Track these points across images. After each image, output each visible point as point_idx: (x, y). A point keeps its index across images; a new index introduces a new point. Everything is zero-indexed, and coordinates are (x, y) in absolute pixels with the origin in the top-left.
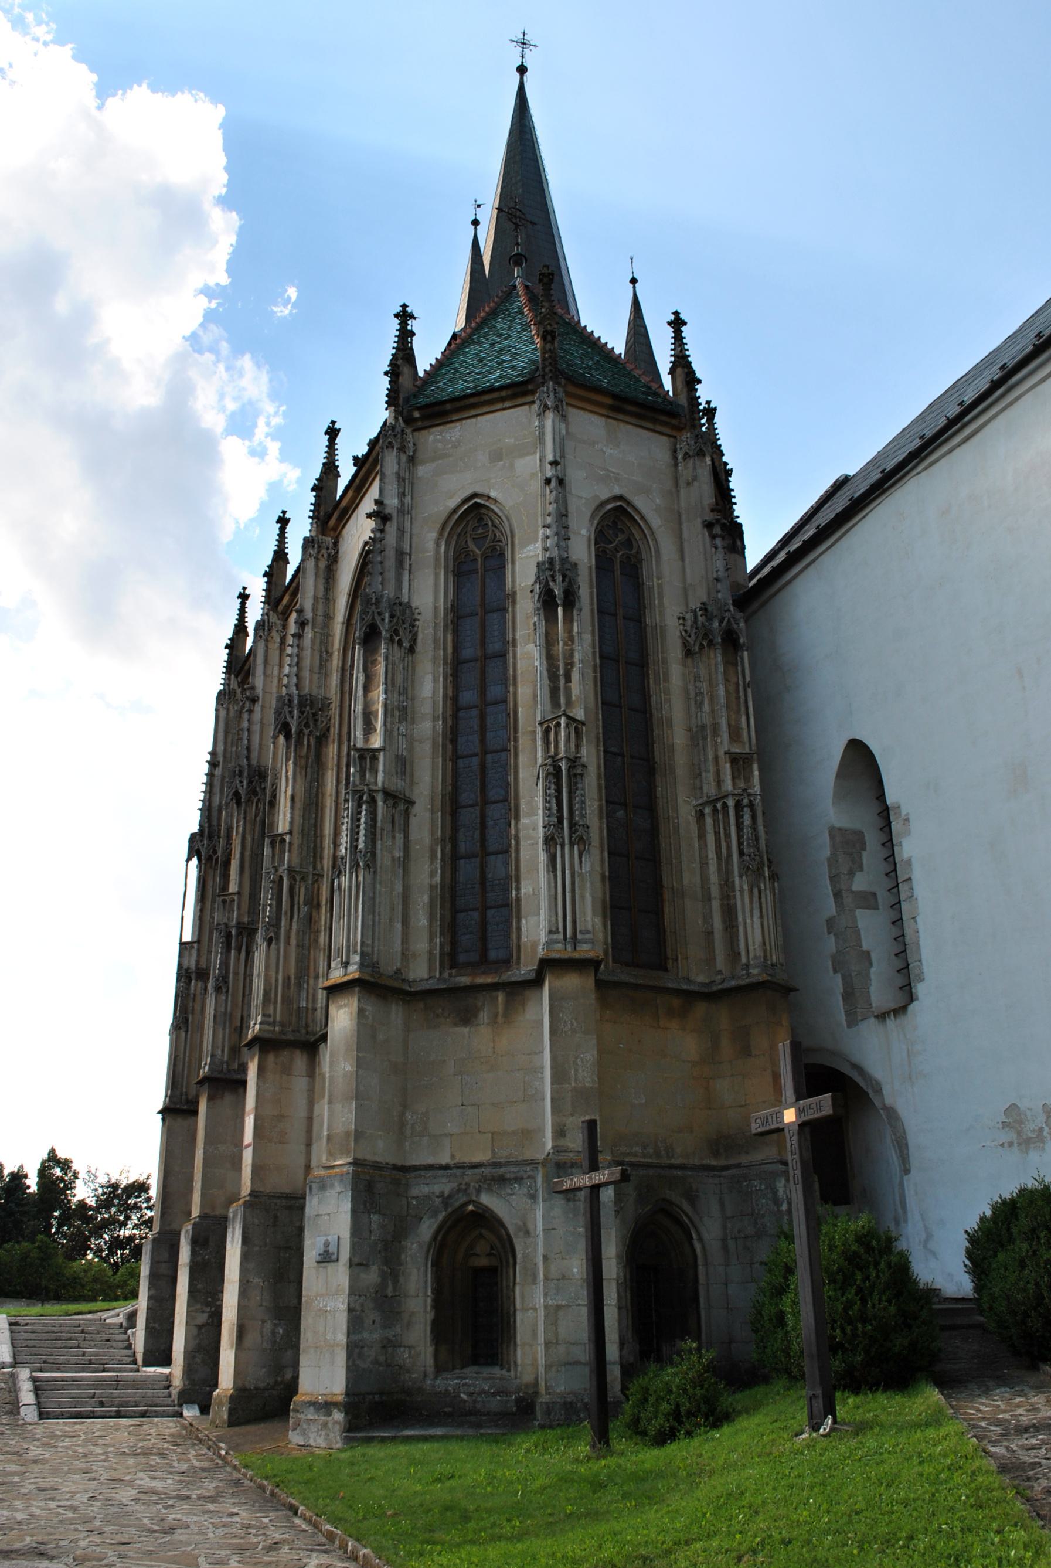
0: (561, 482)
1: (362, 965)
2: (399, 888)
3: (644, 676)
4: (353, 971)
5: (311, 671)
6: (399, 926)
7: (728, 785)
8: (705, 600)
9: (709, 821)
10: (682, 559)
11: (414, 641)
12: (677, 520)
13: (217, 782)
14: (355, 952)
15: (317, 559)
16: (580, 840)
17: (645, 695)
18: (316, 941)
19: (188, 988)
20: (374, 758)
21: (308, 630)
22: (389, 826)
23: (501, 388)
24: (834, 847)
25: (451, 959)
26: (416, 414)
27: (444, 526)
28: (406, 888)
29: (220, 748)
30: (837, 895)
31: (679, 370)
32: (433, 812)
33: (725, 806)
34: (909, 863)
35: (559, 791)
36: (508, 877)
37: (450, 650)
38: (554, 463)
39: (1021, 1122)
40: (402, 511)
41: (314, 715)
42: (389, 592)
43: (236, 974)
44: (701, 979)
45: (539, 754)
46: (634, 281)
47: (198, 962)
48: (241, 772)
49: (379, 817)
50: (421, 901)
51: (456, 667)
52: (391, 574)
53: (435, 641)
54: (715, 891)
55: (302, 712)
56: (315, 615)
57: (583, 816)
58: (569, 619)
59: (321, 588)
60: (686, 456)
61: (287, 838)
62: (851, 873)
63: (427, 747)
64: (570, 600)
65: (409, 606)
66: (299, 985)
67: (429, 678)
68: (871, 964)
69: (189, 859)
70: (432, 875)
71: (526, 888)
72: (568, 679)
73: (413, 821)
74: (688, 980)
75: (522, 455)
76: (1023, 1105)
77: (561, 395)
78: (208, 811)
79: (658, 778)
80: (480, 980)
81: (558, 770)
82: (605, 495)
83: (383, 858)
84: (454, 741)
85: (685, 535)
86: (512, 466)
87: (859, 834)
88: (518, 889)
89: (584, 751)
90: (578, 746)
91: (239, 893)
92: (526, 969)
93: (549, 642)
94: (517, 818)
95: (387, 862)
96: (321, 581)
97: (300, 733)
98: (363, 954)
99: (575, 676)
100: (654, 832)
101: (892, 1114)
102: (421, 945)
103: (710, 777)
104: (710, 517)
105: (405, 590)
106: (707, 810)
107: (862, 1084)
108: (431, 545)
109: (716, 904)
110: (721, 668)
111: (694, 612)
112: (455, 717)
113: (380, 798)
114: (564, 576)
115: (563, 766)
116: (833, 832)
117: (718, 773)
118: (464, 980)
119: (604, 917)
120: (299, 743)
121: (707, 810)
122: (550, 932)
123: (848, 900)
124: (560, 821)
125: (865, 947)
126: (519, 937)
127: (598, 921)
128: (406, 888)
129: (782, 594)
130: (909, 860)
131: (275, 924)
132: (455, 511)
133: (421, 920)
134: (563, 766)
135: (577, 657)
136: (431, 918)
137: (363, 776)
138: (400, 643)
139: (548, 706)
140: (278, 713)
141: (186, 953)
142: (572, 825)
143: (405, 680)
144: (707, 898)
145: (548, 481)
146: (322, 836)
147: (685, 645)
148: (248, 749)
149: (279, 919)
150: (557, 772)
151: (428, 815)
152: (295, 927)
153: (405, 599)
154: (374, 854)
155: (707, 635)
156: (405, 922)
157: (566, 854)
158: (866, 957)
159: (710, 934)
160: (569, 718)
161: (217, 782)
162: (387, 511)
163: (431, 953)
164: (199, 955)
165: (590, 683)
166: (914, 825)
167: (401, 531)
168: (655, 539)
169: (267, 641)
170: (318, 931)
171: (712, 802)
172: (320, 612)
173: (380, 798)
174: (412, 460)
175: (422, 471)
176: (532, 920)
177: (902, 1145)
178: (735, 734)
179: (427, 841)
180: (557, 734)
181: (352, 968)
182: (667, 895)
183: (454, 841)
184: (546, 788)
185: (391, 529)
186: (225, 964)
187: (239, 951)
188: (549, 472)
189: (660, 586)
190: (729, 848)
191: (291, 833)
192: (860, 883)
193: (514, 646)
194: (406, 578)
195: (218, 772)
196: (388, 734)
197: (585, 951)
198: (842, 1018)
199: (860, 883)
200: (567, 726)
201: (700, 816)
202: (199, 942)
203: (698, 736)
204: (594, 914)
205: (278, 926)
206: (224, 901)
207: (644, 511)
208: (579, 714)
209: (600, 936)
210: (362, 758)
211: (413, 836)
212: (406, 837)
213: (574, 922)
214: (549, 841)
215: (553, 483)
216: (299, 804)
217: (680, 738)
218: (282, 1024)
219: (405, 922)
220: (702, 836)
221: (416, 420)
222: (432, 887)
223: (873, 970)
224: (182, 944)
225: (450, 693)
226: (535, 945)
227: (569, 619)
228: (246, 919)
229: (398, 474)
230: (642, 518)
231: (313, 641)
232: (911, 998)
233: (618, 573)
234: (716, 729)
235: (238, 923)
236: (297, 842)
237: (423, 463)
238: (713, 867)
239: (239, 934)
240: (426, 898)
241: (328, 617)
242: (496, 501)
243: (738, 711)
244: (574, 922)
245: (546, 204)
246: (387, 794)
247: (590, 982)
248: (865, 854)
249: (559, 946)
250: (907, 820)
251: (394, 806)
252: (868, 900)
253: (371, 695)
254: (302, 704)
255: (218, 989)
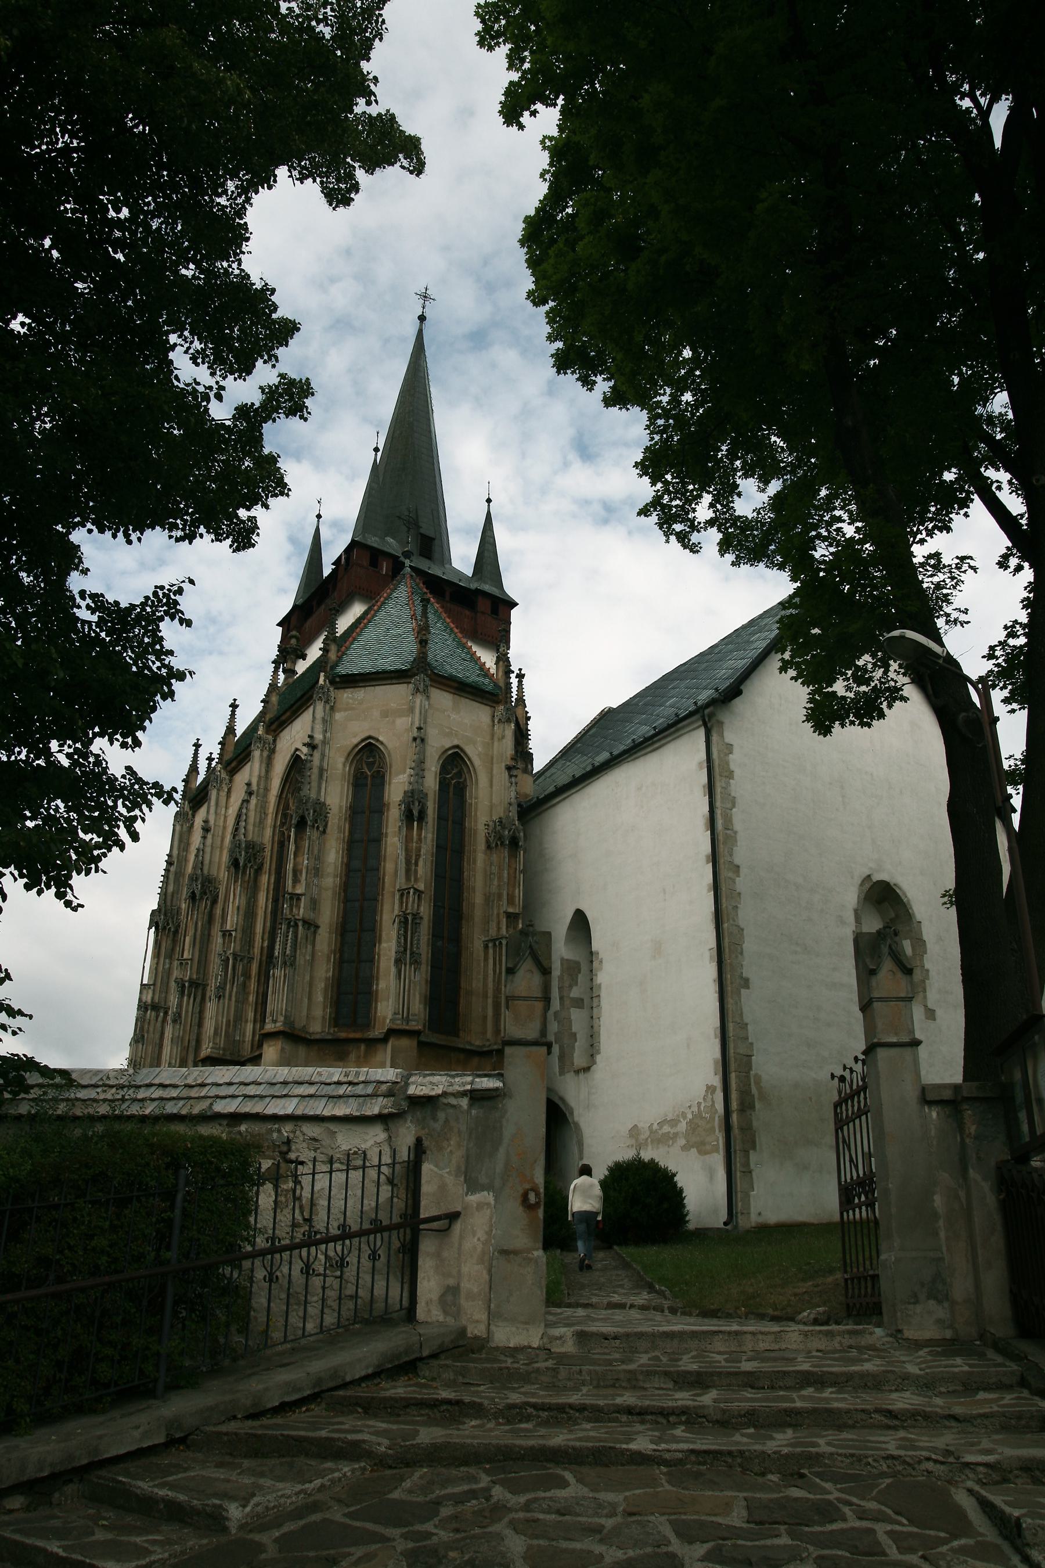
0: (423, 740)
1: (285, 1023)
2: (307, 978)
3: (461, 859)
4: (279, 1026)
5: (254, 825)
6: (306, 1000)
7: (504, 931)
8: (502, 815)
9: (491, 951)
10: (491, 786)
11: (326, 826)
12: (490, 761)
13: (172, 877)
14: (778, 1336)
15: (262, 751)
16: (416, 962)
17: (460, 870)
18: (247, 999)
19: (145, 1015)
20: (299, 899)
21: (253, 797)
22: (304, 941)
23: (391, 672)
24: (562, 971)
25: (336, 1021)
26: (338, 680)
27: (349, 755)
28: (312, 977)
29: (175, 852)
30: (561, 998)
31: (501, 663)
32: (330, 933)
33: (501, 943)
34: (600, 986)
35: (406, 932)
36: (372, 977)
37: (347, 834)
38: (419, 729)
39: (638, 1134)
40: (324, 742)
41: (255, 855)
42: (313, 795)
43: (187, 1011)
44: (478, 1043)
45: (397, 907)
46: (489, 501)
47: (153, 998)
48: (197, 878)
49: (299, 936)
50: (320, 985)
51: (351, 845)
52: (314, 784)
53: (339, 827)
54: (490, 993)
55: (247, 853)
56: (259, 788)
57: (418, 948)
58: (420, 828)
59: (263, 770)
60: (500, 721)
61: (234, 933)
62: (571, 987)
63: (330, 893)
64: (422, 816)
65: (324, 804)
66: (235, 1026)
67: (334, 851)
68: (576, 1040)
69: (149, 929)
70: (327, 971)
71: (382, 985)
72: (416, 864)
73: (318, 938)
74: (470, 1043)
75: (400, 716)
76: (640, 1125)
77: (428, 682)
78: (164, 895)
79: (464, 922)
80: (352, 1035)
81: (406, 919)
82: (447, 746)
83: (300, 960)
84: (345, 891)
85: (495, 772)
86: (394, 722)
87: (578, 963)
88: (377, 985)
89: (422, 909)
90: (418, 906)
91: (191, 960)
92: (377, 1032)
93: (408, 839)
94: (380, 943)
95: (302, 962)
96: (264, 765)
97: (245, 866)
98: (286, 1017)
99: (421, 863)
100: (458, 955)
101: (577, 1125)
102: (318, 1012)
103: (493, 925)
104: (510, 763)
105: (323, 794)
106: (490, 945)
107: (564, 1109)
108: (340, 766)
109: (490, 1001)
110: (507, 860)
111: (494, 822)
112: (347, 875)
113: (300, 924)
114: (420, 802)
115: (410, 918)
116: (562, 959)
117: (499, 923)
118: (343, 1035)
119: (425, 1005)
120: (244, 873)
121: (490, 945)
122: (395, 1014)
123: (567, 1002)
124: (405, 950)
125: (574, 1030)
126: (376, 1013)
127: (422, 1006)
128: (312, 977)
129: (549, 811)
130: (600, 985)
131: (222, 987)
132: (357, 745)
133: (319, 997)
134: (410, 918)
135: (423, 851)
136: (325, 998)
137: (291, 910)
138: (318, 828)
139: (403, 880)
140: (231, 851)
141: (145, 992)
142: (412, 953)
143: (319, 851)
144: (485, 996)
145: (415, 739)
146: (255, 933)
147: (488, 841)
148: (202, 863)
149: (225, 984)
150: (406, 922)
151: (327, 935)
152: (235, 989)
153: (322, 800)
154: (295, 957)
155: (501, 838)
156: (310, 999)
157: (408, 970)
158: (574, 1036)
159: (485, 1018)
160: (415, 889)
161: (172, 877)
162: (316, 742)
163: (324, 1017)
164: (154, 994)
165: (429, 864)
166: (605, 964)
167: (323, 755)
168: (475, 773)
169: (218, 790)
170: (249, 993)
171: (494, 941)
172: (262, 787)
173: (300, 924)
174: (332, 708)
175: (338, 716)
176: (384, 1003)
177: (580, 1144)
178: (511, 901)
179: (326, 951)
180: (407, 898)
181: (278, 1024)
182: (462, 993)
183: (341, 951)
184: (399, 930)
185: (317, 755)
186: (180, 1005)
187: (189, 996)
188: (415, 734)
189: (476, 803)
190: (500, 969)
191: (236, 930)
192: (575, 993)
193: (386, 837)
194: (324, 786)
195: (173, 869)
196: (307, 886)
197: (414, 1026)
198: (557, 1069)
199: (575, 993)
200: (414, 893)
201: (486, 947)
202: (154, 985)
203: (488, 899)
204: (420, 1003)
205: (224, 989)
206: (181, 964)
207: (470, 755)
208: (421, 886)
209: (422, 1016)
210: (291, 898)
211: (317, 947)
212: (314, 946)
213: (408, 1009)
214: (398, 962)
215: (418, 741)
216: (242, 912)
217: (478, 899)
218: (224, 1049)
219: (310, 999)
220: (486, 959)
221: (337, 683)
222: (327, 979)
223: (577, 1044)
224: (142, 985)
225: (345, 860)
226: (385, 1018)
227: (420, 828)
228: (195, 977)
229: (323, 719)
230: (469, 759)
231: (256, 805)
232: (594, 1063)
233: (451, 794)
234: (500, 896)
235: (190, 978)
236: (239, 936)
237: (339, 711)
238: (490, 979)
239: (190, 986)
240: (323, 985)
241: (267, 790)
242: (382, 743)
243: (514, 886)
244: (408, 1009)
245: (430, 432)
246: (305, 922)
247: (415, 1043)
248: (580, 976)
249: (399, 1022)
250: (601, 962)
251: (308, 929)
252: (579, 1003)
253: (300, 859)
254: (247, 847)
255: (174, 1021)
